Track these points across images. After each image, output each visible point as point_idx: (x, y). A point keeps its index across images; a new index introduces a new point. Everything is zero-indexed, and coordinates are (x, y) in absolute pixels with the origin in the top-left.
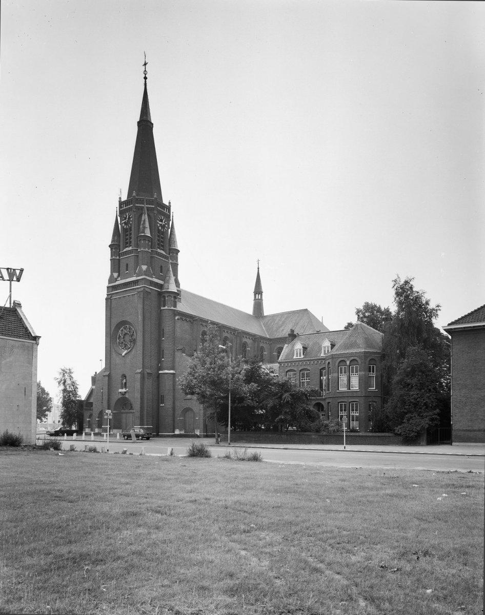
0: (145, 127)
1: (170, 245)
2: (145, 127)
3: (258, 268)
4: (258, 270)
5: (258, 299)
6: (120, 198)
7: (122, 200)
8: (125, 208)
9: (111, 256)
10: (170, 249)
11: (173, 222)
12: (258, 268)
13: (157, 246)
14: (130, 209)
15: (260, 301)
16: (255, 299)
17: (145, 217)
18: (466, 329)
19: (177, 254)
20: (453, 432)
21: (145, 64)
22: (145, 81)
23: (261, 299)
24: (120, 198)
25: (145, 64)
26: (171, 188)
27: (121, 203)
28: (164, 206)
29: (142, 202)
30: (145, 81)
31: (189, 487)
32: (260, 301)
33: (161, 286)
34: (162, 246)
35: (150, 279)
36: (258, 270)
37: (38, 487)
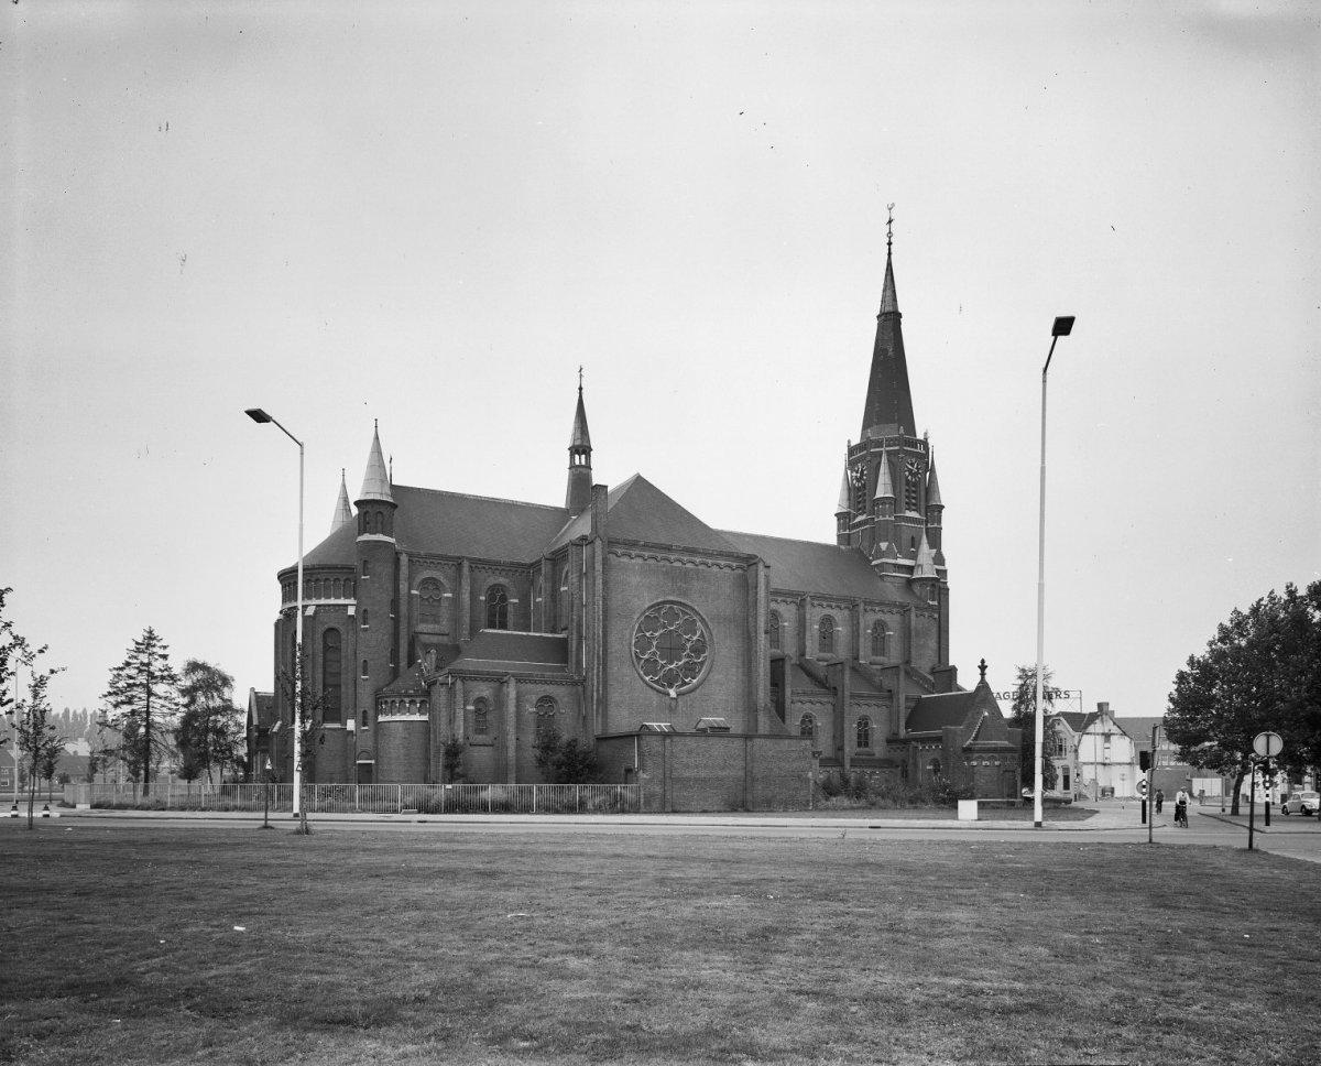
0: (890, 322)
2: (890, 322)
3: (581, 389)
5: (580, 466)
6: (849, 442)
7: (853, 444)
8: (861, 457)
9: (839, 530)
10: (927, 507)
11: (933, 461)
12: (581, 389)
13: (904, 506)
14: (864, 457)
15: (584, 471)
16: (572, 466)
17: (884, 469)
18: (280, 650)
19: (940, 512)
21: (890, 222)
24: (849, 442)
25: (890, 222)
27: (852, 451)
28: (914, 443)
31: (848, 919)
33: (910, 569)
37: (1010, 865)
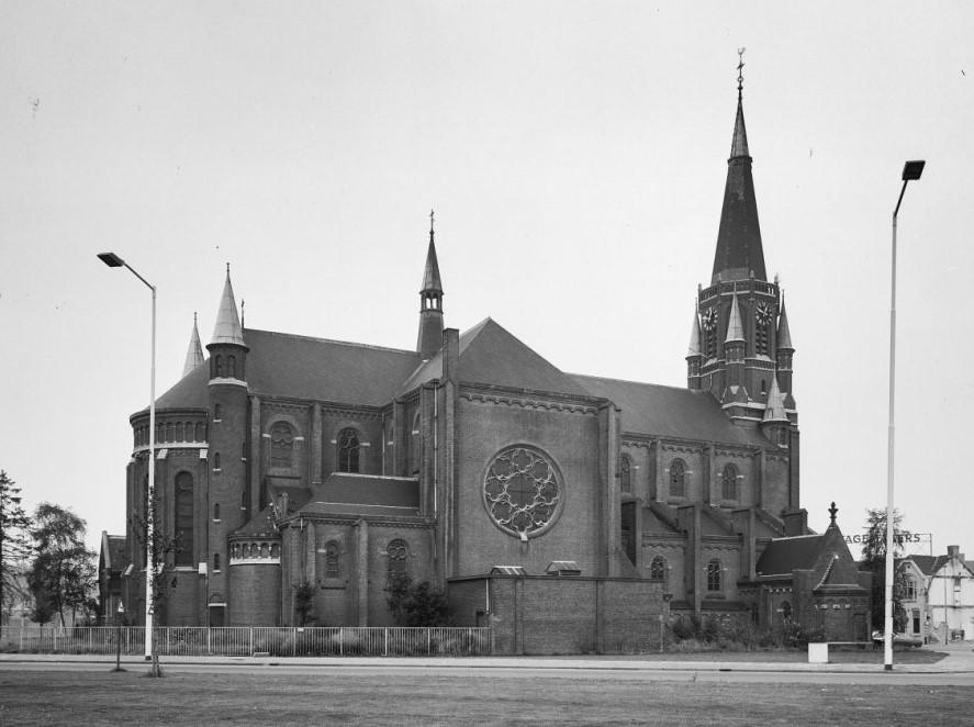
0: (741, 165)
1: (778, 343)
2: (741, 165)
3: (432, 233)
4: (432, 237)
5: (432, 310)
6: (700, 285)
7: (703, 288)
10: (778, 351)
12: (432, 233)
13: (754, 349)
17: (734, 312)
19: (791, 356)
20: (242, 432)
21: (741, 66)
22: (740, 94)
23: (439, 311)
24: (700, 285)
25: (741, 66)
26: (778, 262)
27: (702, 295)
28: (765, 287)
29: (729, 288)
30: (740, 94)
32: (435, 314)
33: (761, 413)
34: (765, 348)
35: (744, 405)
36: (432, 237)
